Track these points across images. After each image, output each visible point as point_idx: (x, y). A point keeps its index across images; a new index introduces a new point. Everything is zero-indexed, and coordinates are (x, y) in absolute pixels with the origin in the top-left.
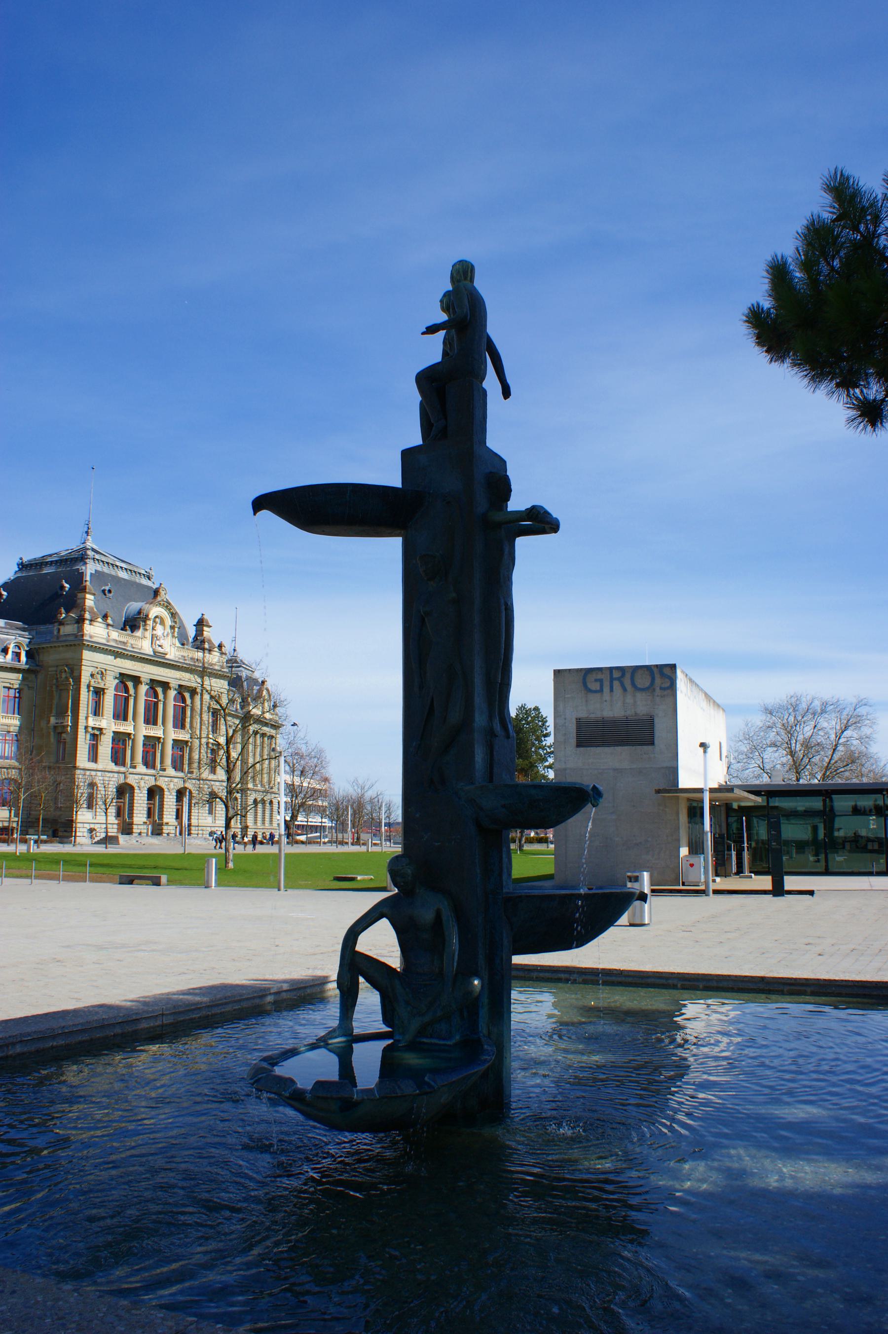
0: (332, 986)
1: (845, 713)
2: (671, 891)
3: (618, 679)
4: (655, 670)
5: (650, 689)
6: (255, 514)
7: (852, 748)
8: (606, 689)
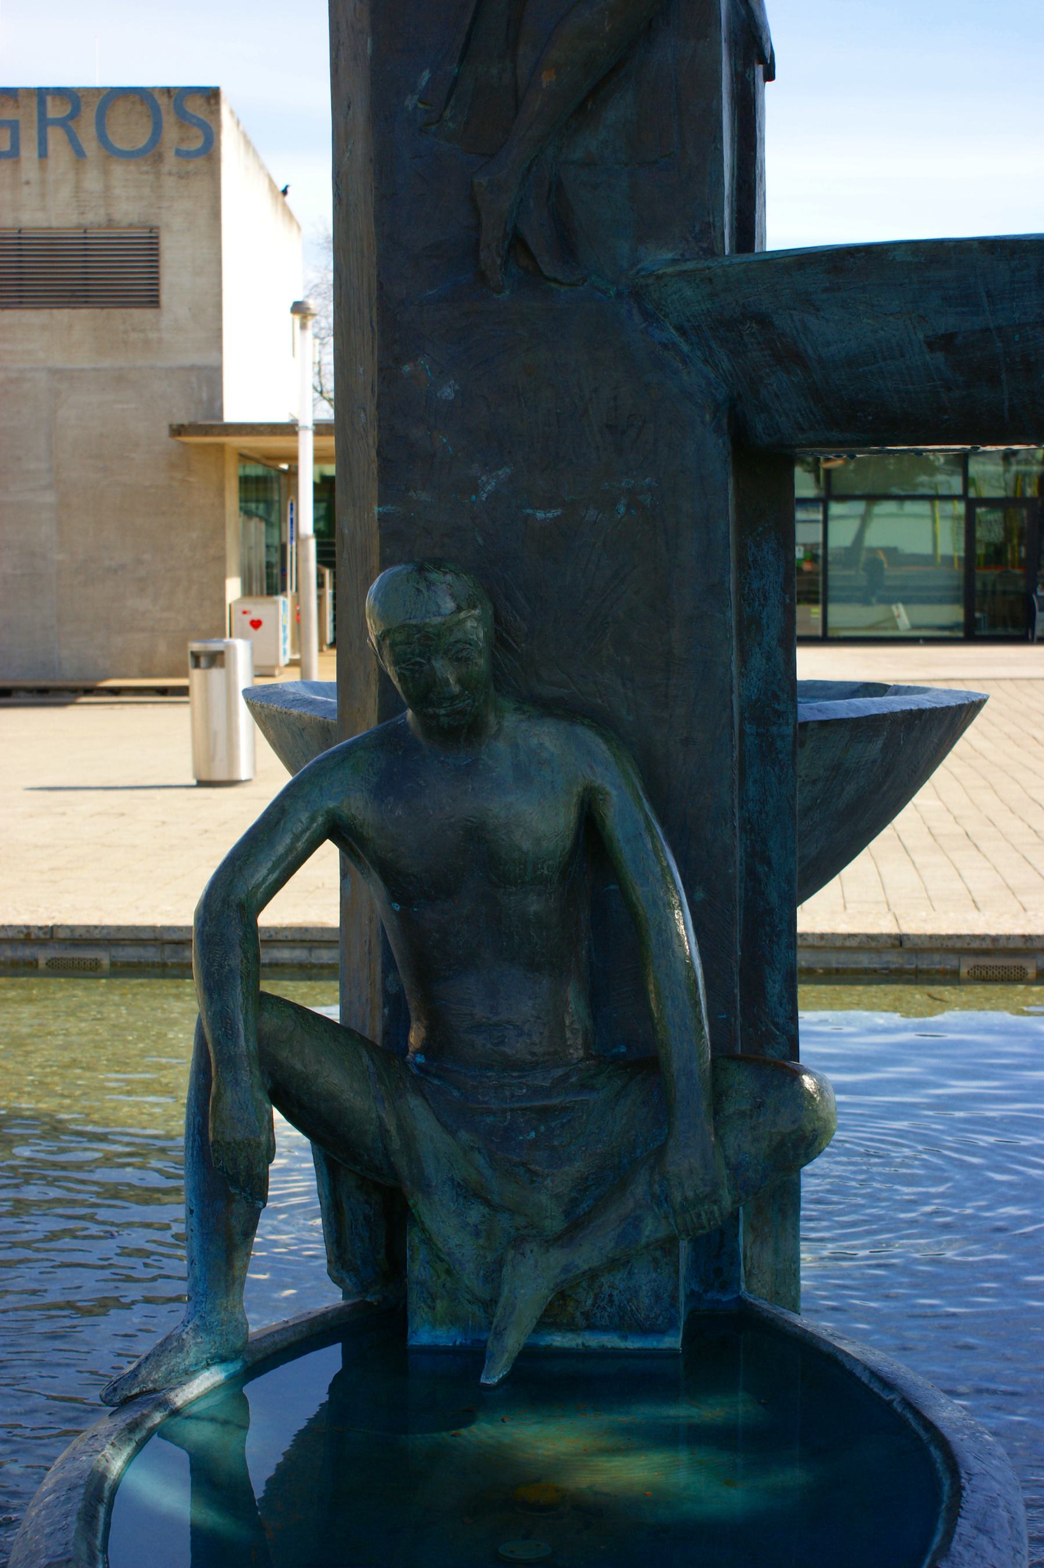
0: (306, 446)
2: (163, 691)
3: (62, 123)
4: (163, 101)
5: (151, 153)
8: (29, 151)
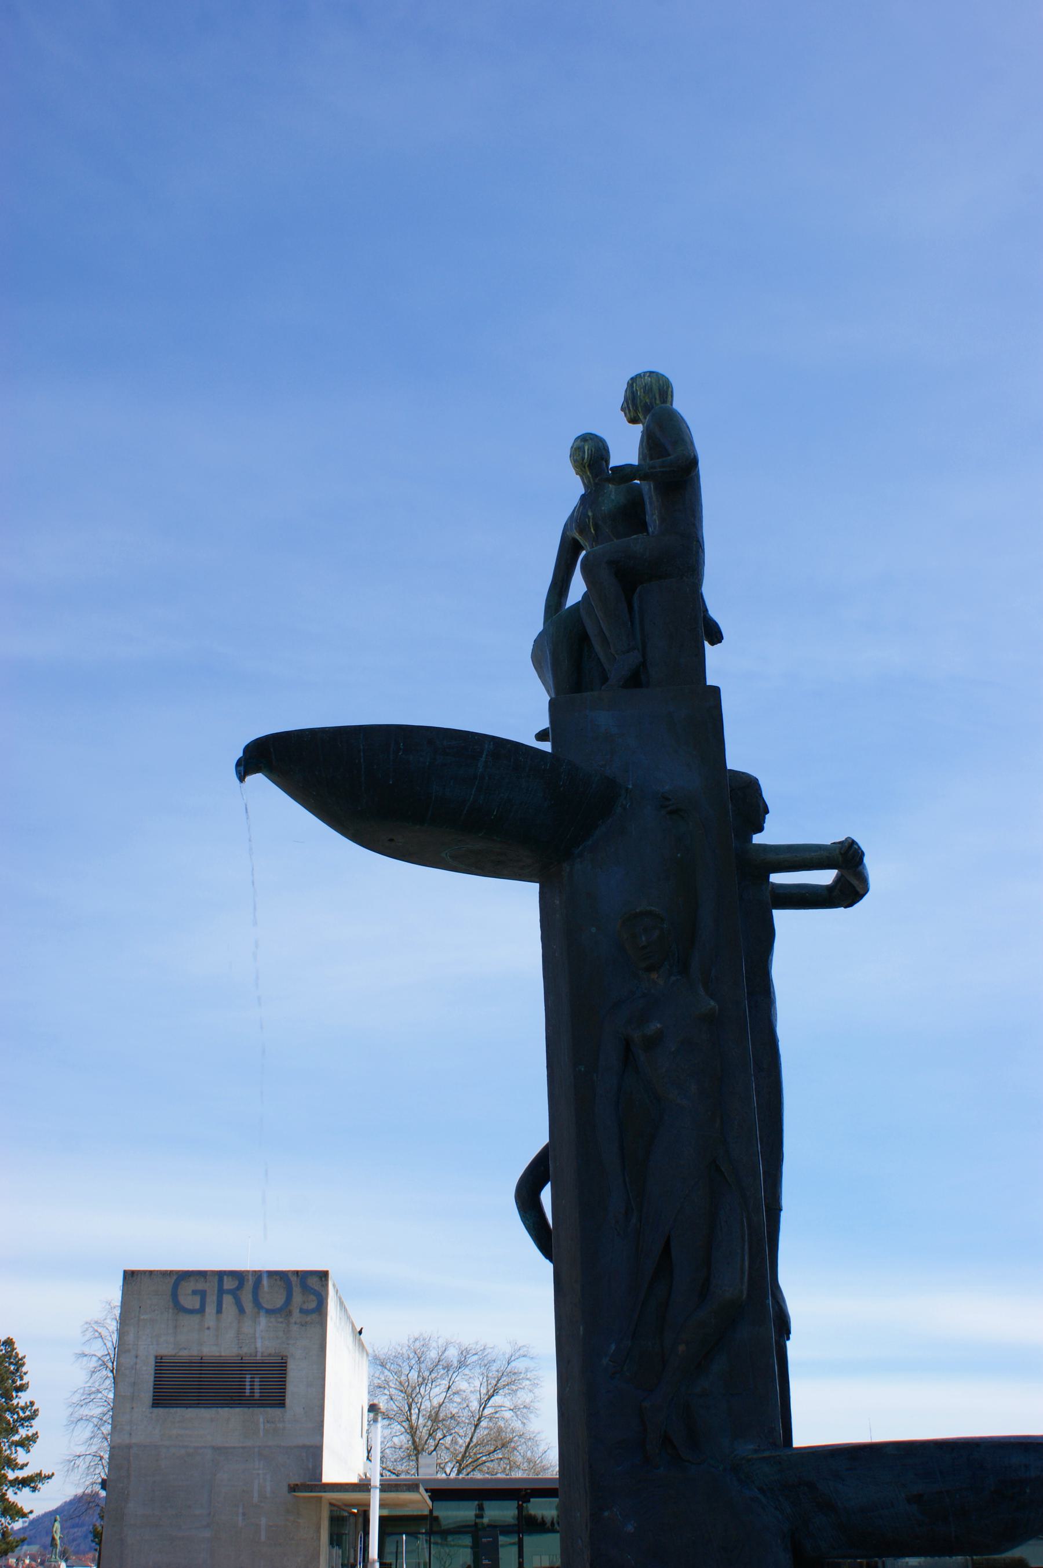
1: (494, 1368)
4: (294, 1279)
5: (284, 1311)
6: (242, 779)
7: (501, 1423)
8: (211, 1309)
